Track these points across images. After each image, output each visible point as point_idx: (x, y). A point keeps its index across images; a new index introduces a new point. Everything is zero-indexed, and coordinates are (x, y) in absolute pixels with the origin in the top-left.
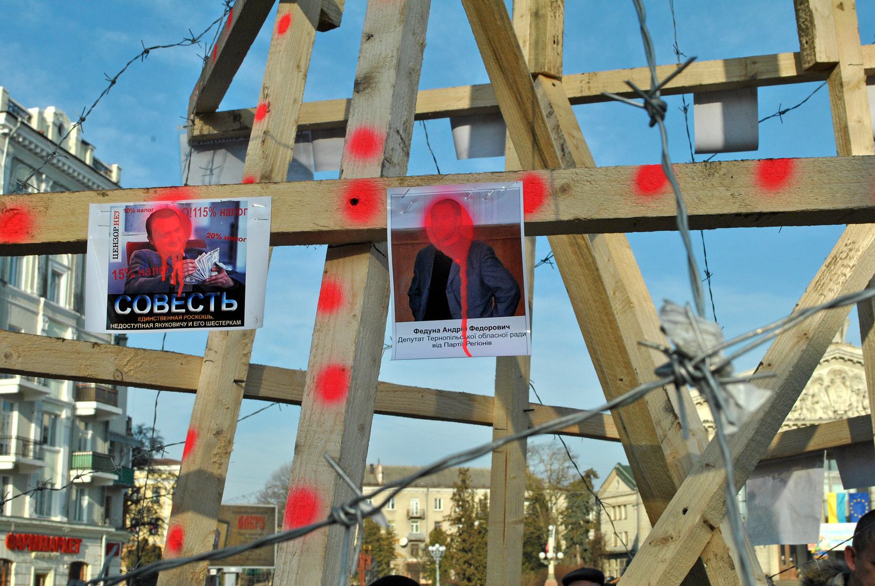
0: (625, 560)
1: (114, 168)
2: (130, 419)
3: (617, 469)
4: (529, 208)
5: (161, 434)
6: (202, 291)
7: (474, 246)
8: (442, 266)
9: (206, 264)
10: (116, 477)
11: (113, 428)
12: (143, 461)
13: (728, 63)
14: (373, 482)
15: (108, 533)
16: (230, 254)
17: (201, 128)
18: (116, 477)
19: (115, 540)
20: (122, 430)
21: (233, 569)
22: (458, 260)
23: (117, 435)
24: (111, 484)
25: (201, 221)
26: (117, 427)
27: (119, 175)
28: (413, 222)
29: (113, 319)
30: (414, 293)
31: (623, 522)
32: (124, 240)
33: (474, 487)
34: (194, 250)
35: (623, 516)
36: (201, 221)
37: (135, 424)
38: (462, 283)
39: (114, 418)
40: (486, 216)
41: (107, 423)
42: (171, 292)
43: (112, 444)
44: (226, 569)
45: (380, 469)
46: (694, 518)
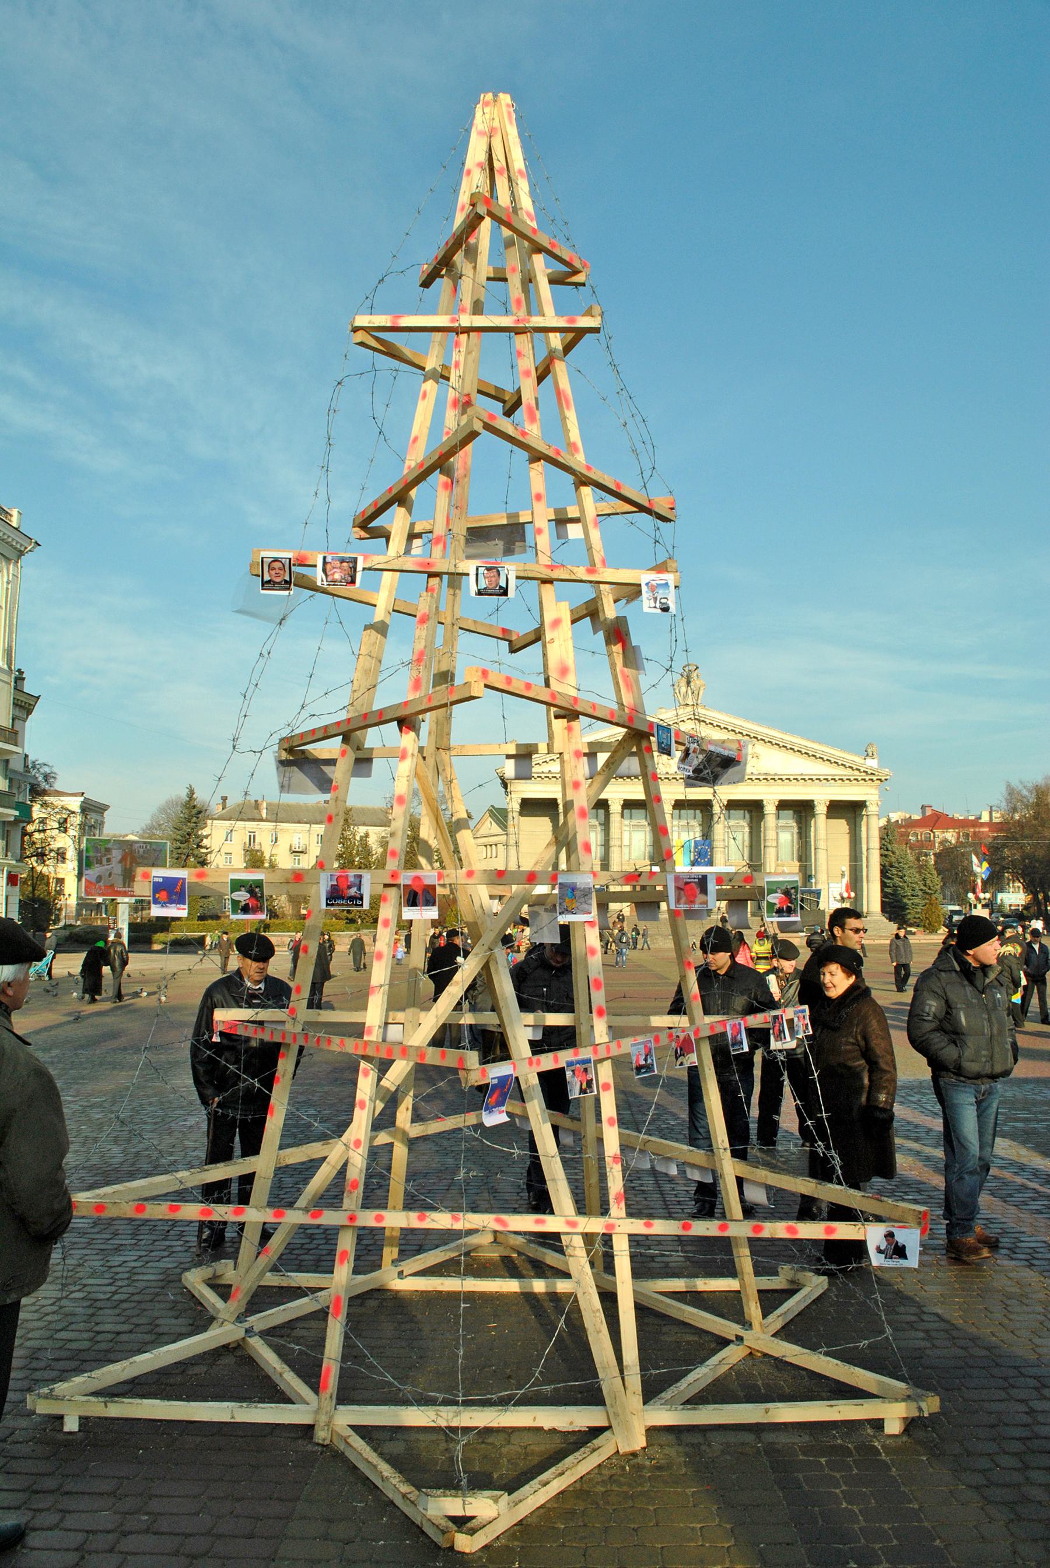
0: (215, 1531)
1: (15, 513)
2: (26, 756)
3: (491, 811)
4: (439, 879)
5: (54, 770)
6: (352, 898)
7: (424, 890)
8: (415, 894)
9: (353, 891)
10: (17, 813)
11: (12, 765)
12: (36, 792)
13: (518, 746)
14: (258, 817)
15: (9, 865)
16: (359, 889)
17: (284, 756)
18: (17, 813)
19: (14, 872)
20: (20, 768)
21: (126, 899)
22: (420, 893)
23: (15, 772)
24: (12, 819)
25: (352, 879)
26: (17, 765)
27: (20, 520)
28: (408, 882)
29: (327, 905)
30: (408, 900)
31: (494, 859)
32: (330, 883)
33: (355, 825)
34: (349, 887)
35: (494, 855)
36: (352, 879)
37: (31, 758)
38: (420, 898)
39: (15, 756)
40: (427, 882)
41: (7, 761)
42: (343, 898)
43: (11, 780)
44: (119, 899)
45: (265, 805)
46: (486, 947)
